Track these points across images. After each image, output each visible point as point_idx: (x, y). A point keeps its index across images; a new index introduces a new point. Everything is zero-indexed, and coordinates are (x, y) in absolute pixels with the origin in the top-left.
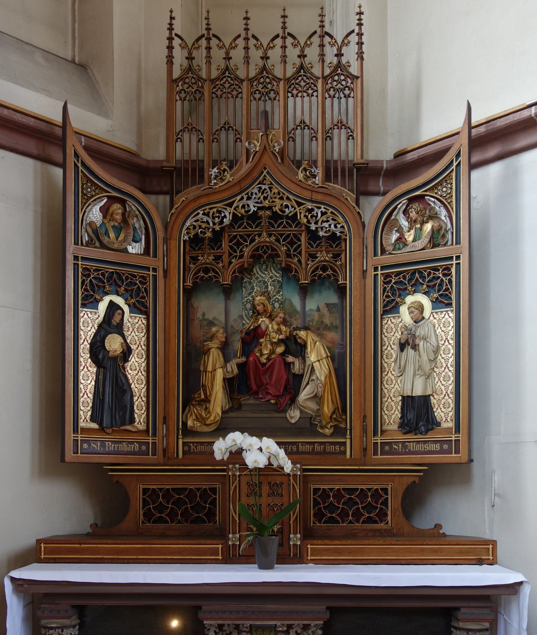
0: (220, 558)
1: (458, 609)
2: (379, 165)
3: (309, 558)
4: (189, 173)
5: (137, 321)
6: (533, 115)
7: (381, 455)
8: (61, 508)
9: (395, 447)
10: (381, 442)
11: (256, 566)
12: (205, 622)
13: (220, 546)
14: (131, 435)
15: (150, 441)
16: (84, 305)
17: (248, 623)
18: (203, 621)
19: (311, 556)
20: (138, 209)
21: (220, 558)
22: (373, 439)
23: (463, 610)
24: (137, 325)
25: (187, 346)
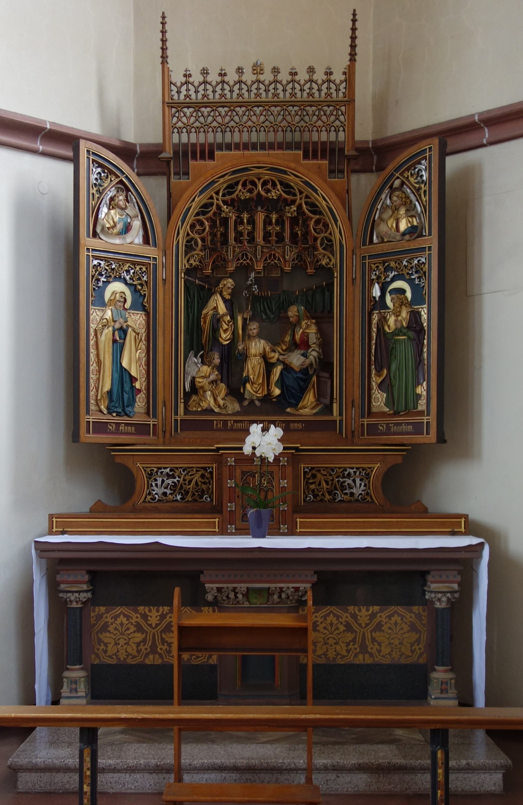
0: (217, 530)
1: (428, 572)
2: (365, 146)
3: (298, 530)
4: (186, 154)
5: (138, 317)
6: (477, 120)
7: (367, 435)
8: (79, 497)
9: (110, 428)
10: (367, 424)
11: (251, 536)
12: (206, 585)
13: (217, 520)
14: (214, 416)
15: (425, 421)
16: (82, 730)
17: (243, 587)
18: (204, 585)
19: (300, 528)
20: (137, 202)
21: (217, 530)
22: (360, 420)
23: (432, 573)
24: (139, 322)
25: (337, 195)
